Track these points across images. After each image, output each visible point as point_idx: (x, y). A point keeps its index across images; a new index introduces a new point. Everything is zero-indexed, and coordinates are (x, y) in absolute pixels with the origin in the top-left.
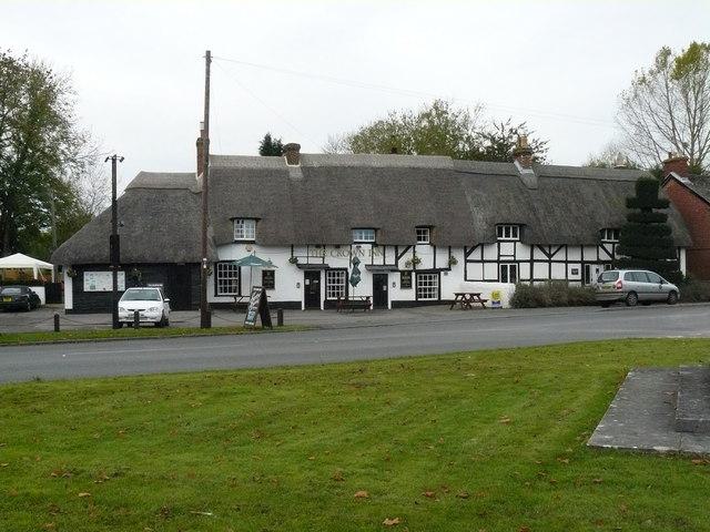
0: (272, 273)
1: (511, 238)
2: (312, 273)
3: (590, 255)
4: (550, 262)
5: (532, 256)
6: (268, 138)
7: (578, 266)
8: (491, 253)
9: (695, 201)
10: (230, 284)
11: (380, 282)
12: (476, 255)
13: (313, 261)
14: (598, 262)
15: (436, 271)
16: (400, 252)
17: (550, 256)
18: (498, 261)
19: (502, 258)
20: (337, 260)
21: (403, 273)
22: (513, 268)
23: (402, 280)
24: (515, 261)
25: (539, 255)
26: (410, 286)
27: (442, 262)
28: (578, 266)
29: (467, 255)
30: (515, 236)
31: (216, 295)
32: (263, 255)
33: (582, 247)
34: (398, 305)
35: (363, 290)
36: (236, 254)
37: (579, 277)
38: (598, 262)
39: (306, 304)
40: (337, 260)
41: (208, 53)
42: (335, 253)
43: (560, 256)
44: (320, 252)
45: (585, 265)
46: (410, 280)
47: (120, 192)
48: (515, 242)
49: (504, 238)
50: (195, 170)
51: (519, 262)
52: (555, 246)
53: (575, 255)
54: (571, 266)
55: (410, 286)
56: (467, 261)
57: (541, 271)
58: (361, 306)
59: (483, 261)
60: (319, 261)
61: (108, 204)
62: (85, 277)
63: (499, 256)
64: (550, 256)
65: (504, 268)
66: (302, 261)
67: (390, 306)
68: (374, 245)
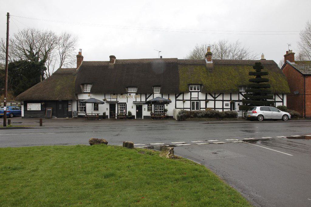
1: (197, 91)
2: (112, 106)
3: (235, 98)
4: (215, 101)
7: (229, 103)
8: (187, 97)
9: (295, 71)
10: (123, 111)
11: (139, 108)
12: (180, 98)
13: (112, 100)
14: (239, 101)
16: (147, 97)
17: (215, 98)
18: (190, 100)
19: (192, 99)
20: (121, 99)
22: (197, 104)
23: (148, 108)
24: (198, 100)
25: (209, 97)
28: (229, 103)
29: (176, 97)
33: (183, 94)
34: (146, 117)
35: (132, 109)
36: (85, 97)
37: (229, 107)
38: (239, 101)
41: (8, 14)
42: (121, 97)
43: (220, 98)
44: (115, 97)
45: (233, 103)
46: (152, 108)
48: (198, 92)
49: (193, 90)
50: (84, 60)
51: (200, 100)
52: (217, 93)
53: (227, 98)
54: (225, 102)
56: (176, 100)
57: (211, 105)
58: (104, 117)
60: (115, 100)
62: (28, 105)
63: (191, 98)
64: (215, 98)
65: (193, 103)
66: (109, 100)
67: (143, 118)
68: (137, 94)
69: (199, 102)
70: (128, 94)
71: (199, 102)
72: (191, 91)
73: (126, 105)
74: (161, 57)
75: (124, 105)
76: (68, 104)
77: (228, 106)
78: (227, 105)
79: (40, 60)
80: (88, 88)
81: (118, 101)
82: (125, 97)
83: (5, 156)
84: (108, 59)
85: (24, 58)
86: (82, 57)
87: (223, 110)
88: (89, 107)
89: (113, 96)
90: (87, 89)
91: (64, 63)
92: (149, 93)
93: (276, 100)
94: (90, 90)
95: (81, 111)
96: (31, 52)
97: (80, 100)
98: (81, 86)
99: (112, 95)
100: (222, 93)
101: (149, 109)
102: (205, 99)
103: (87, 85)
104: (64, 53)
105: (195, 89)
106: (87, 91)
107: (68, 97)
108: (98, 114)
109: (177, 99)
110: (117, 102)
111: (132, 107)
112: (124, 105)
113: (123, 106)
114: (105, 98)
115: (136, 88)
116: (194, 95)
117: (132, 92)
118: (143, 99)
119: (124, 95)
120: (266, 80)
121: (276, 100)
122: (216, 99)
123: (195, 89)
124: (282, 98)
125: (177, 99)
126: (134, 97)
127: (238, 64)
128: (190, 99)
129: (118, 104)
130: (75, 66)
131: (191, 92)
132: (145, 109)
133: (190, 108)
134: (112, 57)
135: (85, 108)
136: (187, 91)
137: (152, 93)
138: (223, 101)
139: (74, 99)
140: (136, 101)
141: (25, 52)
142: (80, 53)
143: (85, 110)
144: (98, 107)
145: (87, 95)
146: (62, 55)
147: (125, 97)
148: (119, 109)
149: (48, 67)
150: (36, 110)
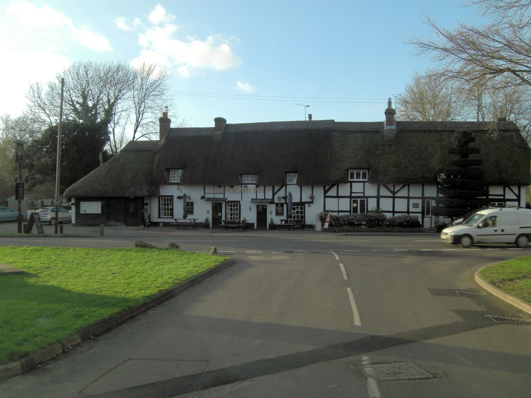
0: (192, 204)
1: (361, 180)
2: (217, 207)
4: (394, 198)
5: (423, 194)
6: (6, 122)
7: (419, 202)
8: (344, 190)
12: (333, 192)
13: (217, 196)
15: (302, 204)
17: (394, 193)
18: (350, 197)
19: (353, 195)
20: (231, 195)
21: (277, 205)
22: (362, 202)
23: (277, 210)
24: (364, 197)
25: (384, 192)
26: (282, 214)
27: (306, 198)
29: (325, 192)
30: (364, 177)
31: (159, 217)
32: (185, 190)
34: (273, 227)
39: (257, 225)
40: (231, 195)
42: (231, 190)
43: (404, 193)
44: (221, 190)
46: (283, 210)
47: (137, 140)
49: (355, 180)
54: (412, 201)
55: (282, 214)
56: (325, 197)
59: (338, 197)
60: (221, 196)
61: (486, 129)
63: (351, 193)
64: (394, 193)
68: (257, 186)
69: (366, 199)
70: (243, 186)
71: (366, 199)
72: (350, 180)
73: (240, 205)
74: (310, 116)
75: (236, 205)
76: (144, 204)
77: (418, 207)
78: (416, 206)
79: (99, 120)
80: (176, 176)
81: (227, 199)
82: (238, 191)
83: (90, 69)
84: (212, 125)
85: (72, 117)
86: (169, 121)
87: (393, 215)
88: (178, 208)
89: (218, 190)
90: (175, 177)
91: (142, 122)
92: (278, 184)
93: (506, 198)
94: (179, 178)
95: (165, 215)
96: (84, 105)
97: (163, 196)
98: (166, 173)
99: (216, 188)
100: (407, 183)
101: (278, 211)
102: (376, 195)
103: (175, 171)
104: (141, 103)
105: (358, 175)
106: (174, 180)
107: (144, 192)
108: (195, 220)
109: (327, 195)
110: (224, 200)
111: (250, 208)
112: (237, 205)
113: (234, 206)
114: (205, 193)
115: (256, 175)
116: (357, 188)
117: (250, 182)
118: (269, 196)
119: (236, 187)
120: (478, 162)
121: (506, 198)
122: (396, 195)
123: (358, 175)
124: (517, 194)
125: (327, 195)
126: (252, 191)
127: (444, 129)
128: (349, 195)
129: (226, 202)
130: (156, 138)
131: (351, 182)
132: (271, 212)
133: (350, 212)
134: (219, 121)
135: (172, 209)
136: (344, 180)
137: (284, 184)
138: (408, 198)
139: (154, 193)
140: (256, 199)
141: (73, 105)
142: (165, 114)
143: (172, 214)
144: (193, 208)
145: (175, 187)
146: (138, 107)
147: (238, 191)
148: (229, 211)
149: (114, 131)
150: (94, 213)
